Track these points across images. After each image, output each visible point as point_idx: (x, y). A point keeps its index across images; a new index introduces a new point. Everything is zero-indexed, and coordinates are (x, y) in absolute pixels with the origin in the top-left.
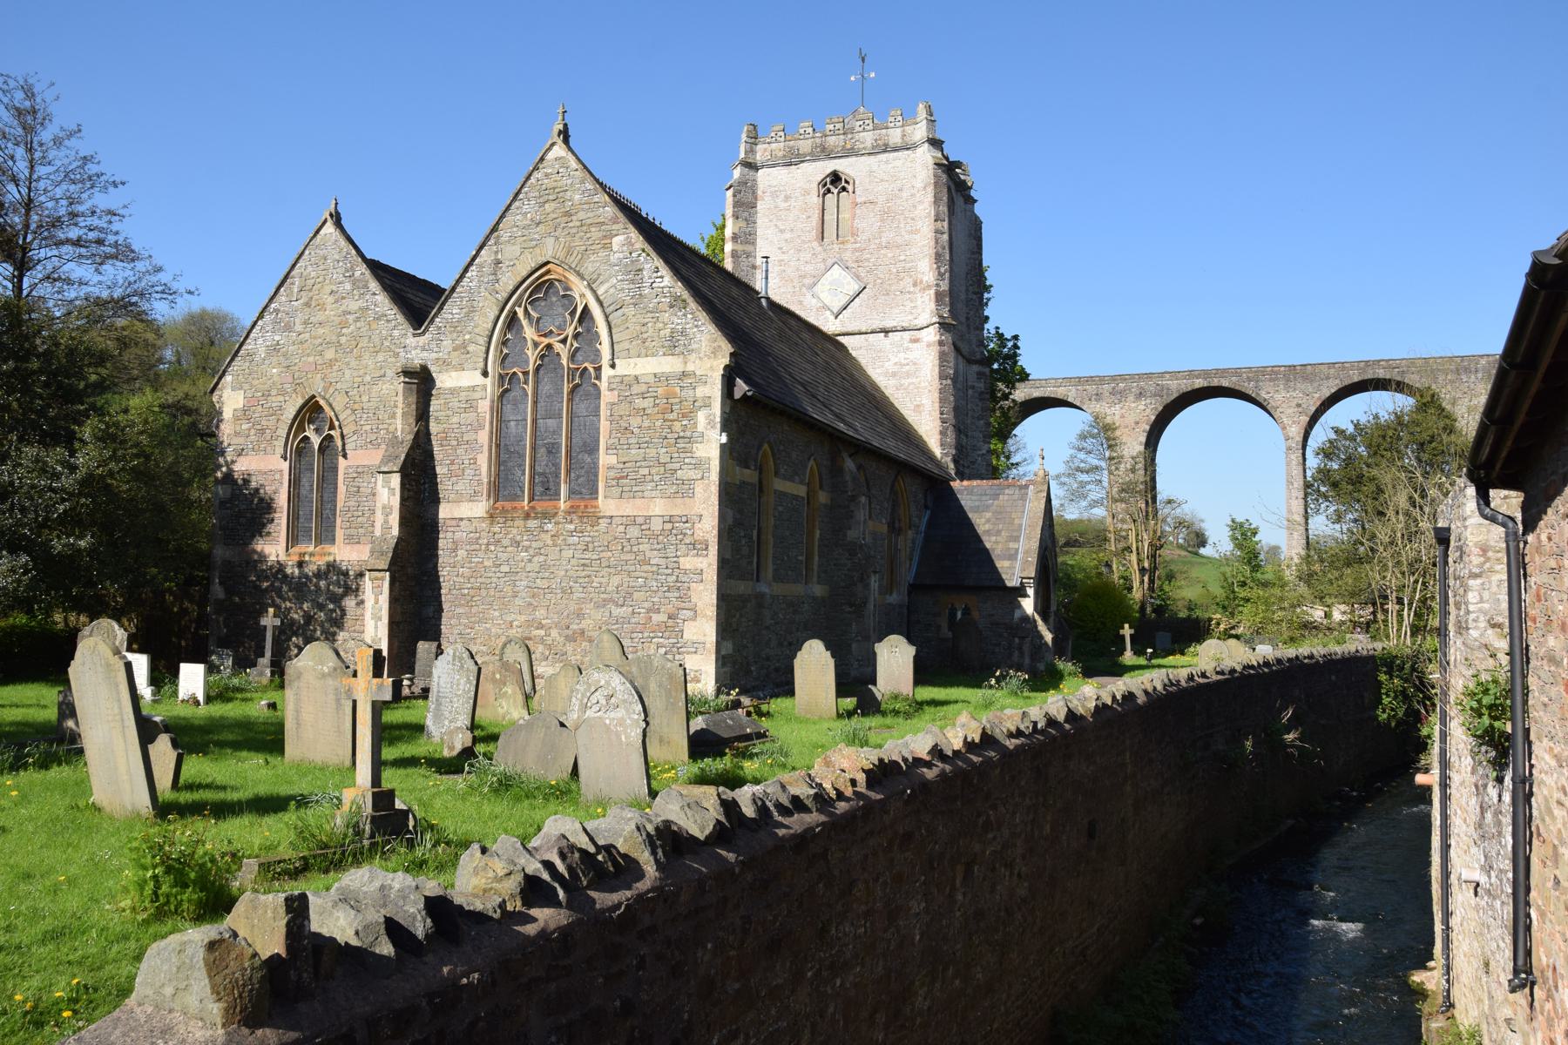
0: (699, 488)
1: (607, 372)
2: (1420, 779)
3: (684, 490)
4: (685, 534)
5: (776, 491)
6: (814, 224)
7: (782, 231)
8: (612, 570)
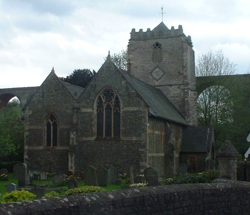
1: (122, 110)
5: (156, 134)
7: (143, 58)
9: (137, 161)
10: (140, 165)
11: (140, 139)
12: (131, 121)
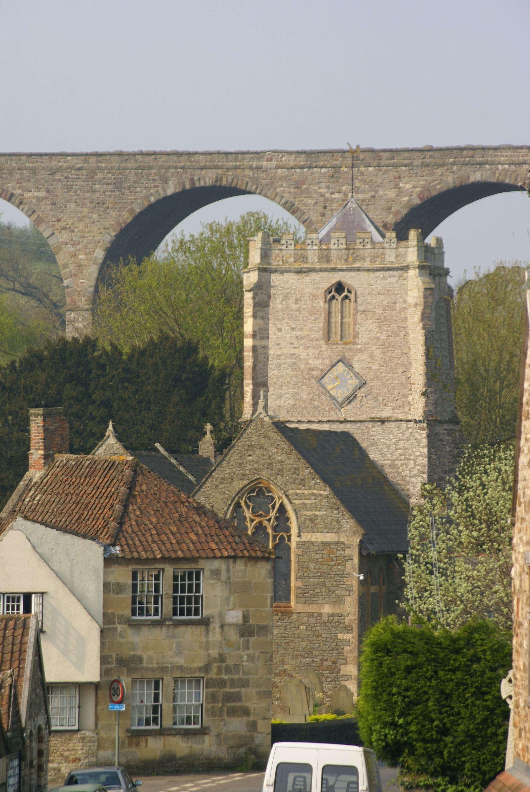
0: (348, 599)
1: (294, 539)
2: (300, 584)
3: (339, 601)
4: (340, 622)
6: (321, 325)
7: (293, 329)
8: (301, 640)
9: (334, 663)
10: (342, 672)
11: (341, 611)
12: (318, 567)
